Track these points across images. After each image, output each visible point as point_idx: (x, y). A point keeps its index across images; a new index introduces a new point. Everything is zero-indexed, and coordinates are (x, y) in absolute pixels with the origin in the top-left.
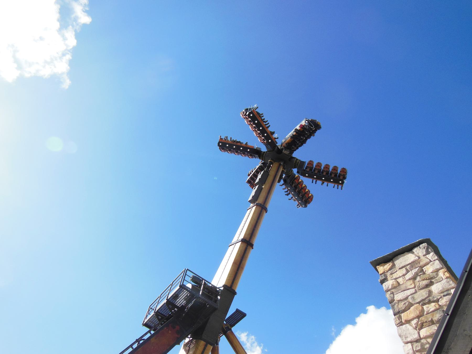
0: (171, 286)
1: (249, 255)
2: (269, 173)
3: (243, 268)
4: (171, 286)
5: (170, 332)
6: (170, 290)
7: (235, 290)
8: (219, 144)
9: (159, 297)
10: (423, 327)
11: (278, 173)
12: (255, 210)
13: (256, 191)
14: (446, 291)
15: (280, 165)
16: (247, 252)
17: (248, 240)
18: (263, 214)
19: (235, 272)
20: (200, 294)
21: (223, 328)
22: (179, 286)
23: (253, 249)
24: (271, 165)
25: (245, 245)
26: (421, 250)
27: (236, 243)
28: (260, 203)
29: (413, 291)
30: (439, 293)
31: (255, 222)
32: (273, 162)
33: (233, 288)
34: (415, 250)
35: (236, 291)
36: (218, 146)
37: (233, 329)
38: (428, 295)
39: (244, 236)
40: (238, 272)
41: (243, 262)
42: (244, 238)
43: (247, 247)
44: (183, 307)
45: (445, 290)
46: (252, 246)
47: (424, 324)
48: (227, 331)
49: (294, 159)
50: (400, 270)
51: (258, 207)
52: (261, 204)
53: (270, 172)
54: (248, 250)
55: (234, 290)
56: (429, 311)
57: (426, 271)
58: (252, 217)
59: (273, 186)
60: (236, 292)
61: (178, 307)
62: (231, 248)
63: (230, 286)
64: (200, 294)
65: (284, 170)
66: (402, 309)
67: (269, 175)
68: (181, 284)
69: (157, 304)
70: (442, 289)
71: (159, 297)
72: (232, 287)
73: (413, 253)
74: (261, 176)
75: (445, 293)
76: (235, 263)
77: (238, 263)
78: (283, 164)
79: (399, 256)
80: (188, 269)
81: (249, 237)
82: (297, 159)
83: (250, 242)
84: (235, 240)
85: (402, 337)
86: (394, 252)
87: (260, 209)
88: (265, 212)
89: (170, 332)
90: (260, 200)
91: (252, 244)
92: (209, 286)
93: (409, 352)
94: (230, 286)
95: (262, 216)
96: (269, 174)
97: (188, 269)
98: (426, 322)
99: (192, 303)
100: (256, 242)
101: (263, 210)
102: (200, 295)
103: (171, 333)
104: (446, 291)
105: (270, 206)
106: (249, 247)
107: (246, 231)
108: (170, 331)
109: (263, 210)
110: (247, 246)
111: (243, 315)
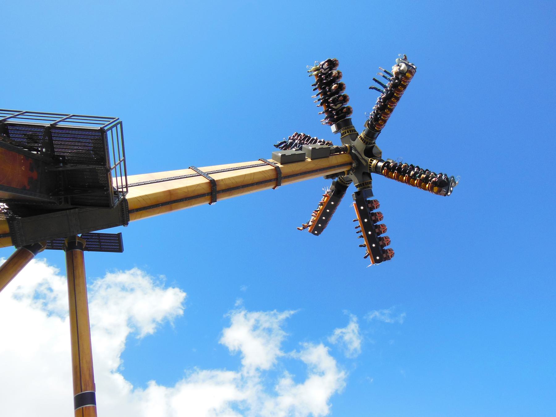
2: (330, 155)
3: (171, 209)
5: (24, 169)
7: (129, 220)
13: (295, 154)
15: (351, 164)
17: (218, 188)
23: (210, 204)
25: (207, 190)
31: (250, 183)
32: (348, 151)
35: (130, 222)
39: (219, 180)
43: (207, 195)
58: (254, 173)
59: (316, 173)
60: (127, 224)
61: (54, 152)
63: (129, 209)
65: (346, 173)
69: (60, 119)
74: (320, 148)
76: (170, 193)
81: (224, 188)
83: (217, 195)
84: (204, 169)
90: (286, 169)
95: (266, 186)
97: (121, 123)
100: (223, 200)
106: (209, 197)
108: (24, 167)
110: (208, 194)
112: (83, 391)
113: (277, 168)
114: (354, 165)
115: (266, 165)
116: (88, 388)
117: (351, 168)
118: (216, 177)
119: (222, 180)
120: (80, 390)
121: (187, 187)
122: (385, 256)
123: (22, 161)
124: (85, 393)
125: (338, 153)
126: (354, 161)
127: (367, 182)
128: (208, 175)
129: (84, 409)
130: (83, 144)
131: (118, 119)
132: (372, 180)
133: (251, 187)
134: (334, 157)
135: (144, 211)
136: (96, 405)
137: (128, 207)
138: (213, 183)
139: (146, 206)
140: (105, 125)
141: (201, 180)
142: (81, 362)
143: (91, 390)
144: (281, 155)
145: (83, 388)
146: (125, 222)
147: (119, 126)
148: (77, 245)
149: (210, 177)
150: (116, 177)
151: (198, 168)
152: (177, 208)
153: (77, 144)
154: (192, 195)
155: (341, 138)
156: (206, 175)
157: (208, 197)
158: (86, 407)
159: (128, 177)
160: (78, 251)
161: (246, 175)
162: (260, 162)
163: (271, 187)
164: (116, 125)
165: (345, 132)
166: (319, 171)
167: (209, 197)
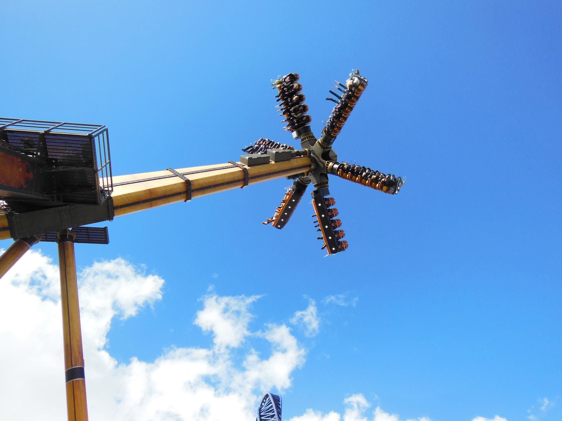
1: (258, 181)
2: (292, 158)
5: (21, 171)
6: (13, 124)
7: (114, 216)
8: (280, 228)
11: (298, 170)
12: (235, 172)
13: (260, 158)
15: (310, 166)
16: (176, 197)
17: (193, 188)
18: (238, 185)
19: (140, 200)
23: (186, 202)
24: (302, 156)
25: (183, 189)
27: (238, 166)
28: (249, 172)
31: (221, 182)
35: (115, 217)
36: (281, 229)
39: (194, 180)
40: (2, 231)
41: (160, 201)
42: (192, 181)
43: (183, 194)
46: (188, 198)
49: (326, 179)
51: (242, 174)
52: (248, 174)
53: (293, 160)
54: (179, 197)
55: (114, 214)
57: (284, 202)
58: (224, 174)
59: (280, 174)
60: (112, 219)
65: (306, 174)
67: (290, 161)
68: (93, 135)
72: (116, 209)
74: (282, 152)
76: (150, 191)
77: (153, 196)
78: (312, 169)
81: (198, 187)
82: (327, 183)
84: (180, 171)
87: (241, 178)
88: (241, 186)
89: (20, 170)
91: (248, 183)
94: (114, 206)
96: (290, 160)
97: (107, 130)
100: (197, 198)
101: (243, 182)
103: (20, 171)
105: (252, 184)
106: (185, 195)
107: (202, 179)
108: (21, 168)
109: (243, 182)
110: (184, 193)
111: (105, 240)
112: (73, 366)
113: (245, 170)
114: (313, 167)
115: (235, 167)
117: (310, 170)
118: (191, 178)
119: (196, 180)
120: (71, 366)
121: (165, 186)
122: (340, 247)
123: (20, 164)
124: (76, 368)
125: (299, 157)
126: (312, 164)
128: (184, 176)
129: (74, 382)
131: (105, 126)
132: (328, 180)
133: (221, 187)
134: (295, 160)
135: (127, 208)
136: (84, 378)
137: (113, 204)
140: (93, 132)
141: (178, 180)
142: (71, 340)
143: (81, 366)
145: (73, 363)
146: (110, 217)
147: (105, 133)
151: (175, 170)
153: (68, 148)
154: (170, 193)
155: (301, 144)
156: (182, 176)
158: (76, 380)
159: (113, 177)
161: (217, 176)
162: (230, 164)
163: (239, 187)
165: (305, 138)
167: (185, 195)
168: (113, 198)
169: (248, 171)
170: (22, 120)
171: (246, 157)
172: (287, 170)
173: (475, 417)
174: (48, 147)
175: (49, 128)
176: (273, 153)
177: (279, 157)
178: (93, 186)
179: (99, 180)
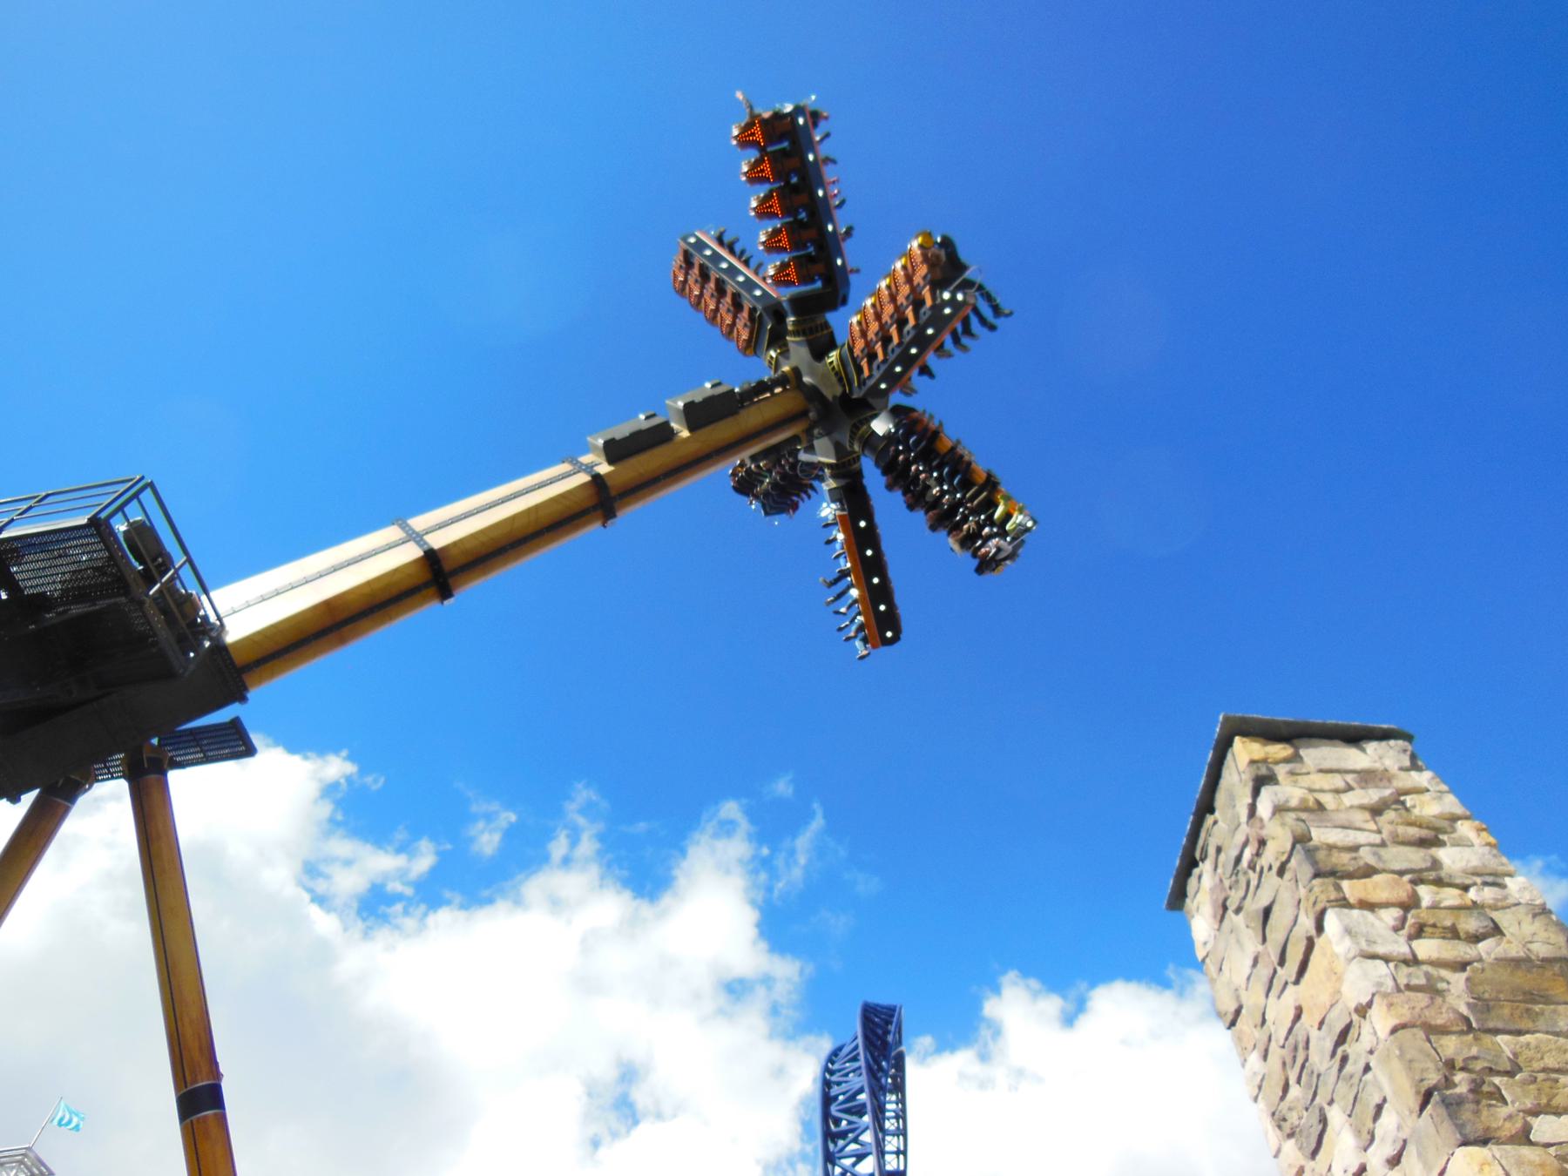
0: (31, 503)
3: (343, 641)
4: (31, 503)
9: (35, 497)
10: (1424, 935)
14: (1490, 874)
15: (803, 414)
20: (151, 593)
21: (141, 753)
22: (89, 516)
25: (424, 575)
26: (1391, 753)
29: (1376, 839)
30: (1467, 874)
33: (247, 678)
34: (1372, 747)
37: (174, 776)
38: (1429, 864)
42: (443, 549)
44: (41, 602)
45: (1488, 871)
47: (1426, 929)
48: (147, 772)
50: (1321, 775)
56: (1440, 902)
61: (21, 590)
62: (565, 467)
64: (151, 593)
66: (1344, 868)
68: (103, 515)
70: (1480, 865)
71: (35, 497)
73: (1363, 750)
75: (1490, 879)
76: (328, 606)
79: (1315, 741)
80: (151, 485)
85: (1355, 936)
86: (1308, 725)
92: (178, 590)
93: (1382, 980)
97: (151, 485)
98: (1434, 926)
99: (95, 605)
100: (472, 594)
102: (147, 595)
104: (1490, 874)
110: (594, 508)
113: (597, 478)
116: (199, 1077)
118: (438, 541)
119: (455, 544)
125: (768, 395)
127: (849, 460)
129: (195, 1122)
130: (30, 575)
131: (142, 478)
134: (753, 409)
136: (224, 1108)
137: (232, 663)
138: (431, 557)
139: (269, 665)
140: (102, 506)
143: (208, 1080)
144: (602, 442)
145: (188, 1078)
146: (238, 694)
148: (146, 766)
149: (426, 543)
150: (207, 593)
152: (356, 634)
153: (59, 561)
157: (599, 512)
159: (212, 594)
160: (827, 457)
164: (136, 496)
166: (664, 479)
167: (599, 512)
168: (231, 651)
169: (606, 479)
170: (44, 494)
171: (596, 440)
172: (559, 480)
173: (1128, 978)
174: (101, 546)
175: (116, 492)
176: (678, 410)
177: (697, 414)
178: (151, 637)
179: (585, 524)
